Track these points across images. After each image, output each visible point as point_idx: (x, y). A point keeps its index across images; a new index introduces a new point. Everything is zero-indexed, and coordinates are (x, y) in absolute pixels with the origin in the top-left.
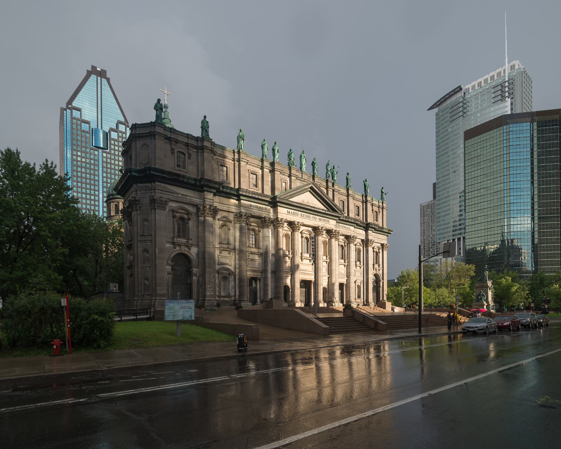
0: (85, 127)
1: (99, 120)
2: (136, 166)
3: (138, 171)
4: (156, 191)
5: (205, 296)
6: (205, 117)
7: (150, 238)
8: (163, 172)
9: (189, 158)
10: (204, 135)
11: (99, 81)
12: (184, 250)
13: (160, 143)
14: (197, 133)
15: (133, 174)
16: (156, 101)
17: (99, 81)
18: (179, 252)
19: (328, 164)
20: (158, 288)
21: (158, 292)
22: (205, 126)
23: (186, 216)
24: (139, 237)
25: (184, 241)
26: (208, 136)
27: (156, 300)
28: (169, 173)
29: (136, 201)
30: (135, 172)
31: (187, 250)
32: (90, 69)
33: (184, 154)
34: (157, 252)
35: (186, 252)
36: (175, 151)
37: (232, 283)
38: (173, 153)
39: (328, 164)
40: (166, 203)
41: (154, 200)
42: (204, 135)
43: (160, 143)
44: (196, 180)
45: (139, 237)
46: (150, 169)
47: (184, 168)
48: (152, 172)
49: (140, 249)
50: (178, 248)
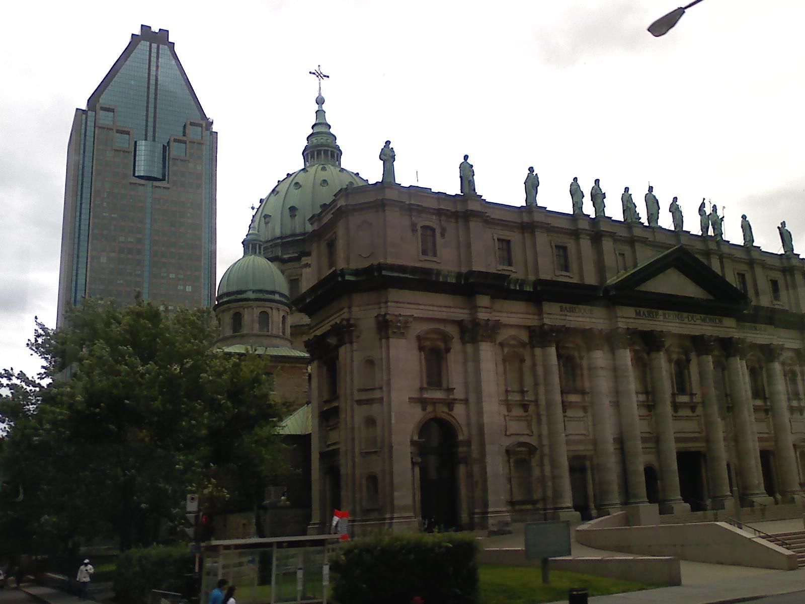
0: (121, 141)
1: (150, 124)
2: (348, 262)
3: (356, 273)
4: (389, 304)
5: (486, 504)
6: (466, 157)
7: (377, 394)
8: (402, 269)
9: (443, 235)
10: (466, 190)
11: (154, 50)
12: (442, 411)
13: (394, 217)
14: (453, 187)
15: (348, 278)
16: (382, 145)
17: (154, 50)
18: (431, 416)
19: (703, 205)
20: (396, 494)
21: (396, 502)
22: (467, 173)
23: (441, 345)
24: (356, 393)
25: (438, 395)
26: (474, 190)
27: (392, 518)
28: (414, 270)
29: (352, 325)
30: (351, 274)
31: (446, 409)
32: (138, 31)
33: (433, 230)
34: (393, 421)
35: (444, 416)
36: (418, 227)
37: (536, 472)
38: (414, 230)
39: (703, 205)
40: (406, 325)
41: (386, 321)
42: (466, 190)
43: (394, 217)
44: (459, 275)
45: (356, 393)
46: (380, 267)
47: (435, 255)
48: (384, 273)
49: (358, 420)
50: (429, 409)
